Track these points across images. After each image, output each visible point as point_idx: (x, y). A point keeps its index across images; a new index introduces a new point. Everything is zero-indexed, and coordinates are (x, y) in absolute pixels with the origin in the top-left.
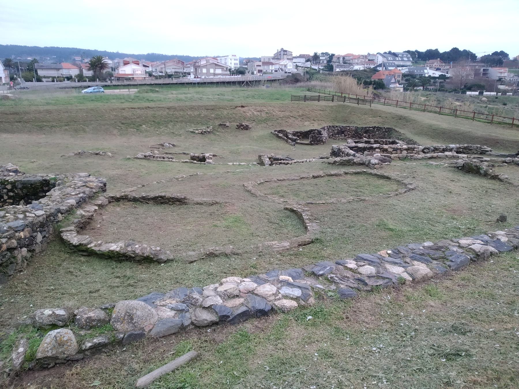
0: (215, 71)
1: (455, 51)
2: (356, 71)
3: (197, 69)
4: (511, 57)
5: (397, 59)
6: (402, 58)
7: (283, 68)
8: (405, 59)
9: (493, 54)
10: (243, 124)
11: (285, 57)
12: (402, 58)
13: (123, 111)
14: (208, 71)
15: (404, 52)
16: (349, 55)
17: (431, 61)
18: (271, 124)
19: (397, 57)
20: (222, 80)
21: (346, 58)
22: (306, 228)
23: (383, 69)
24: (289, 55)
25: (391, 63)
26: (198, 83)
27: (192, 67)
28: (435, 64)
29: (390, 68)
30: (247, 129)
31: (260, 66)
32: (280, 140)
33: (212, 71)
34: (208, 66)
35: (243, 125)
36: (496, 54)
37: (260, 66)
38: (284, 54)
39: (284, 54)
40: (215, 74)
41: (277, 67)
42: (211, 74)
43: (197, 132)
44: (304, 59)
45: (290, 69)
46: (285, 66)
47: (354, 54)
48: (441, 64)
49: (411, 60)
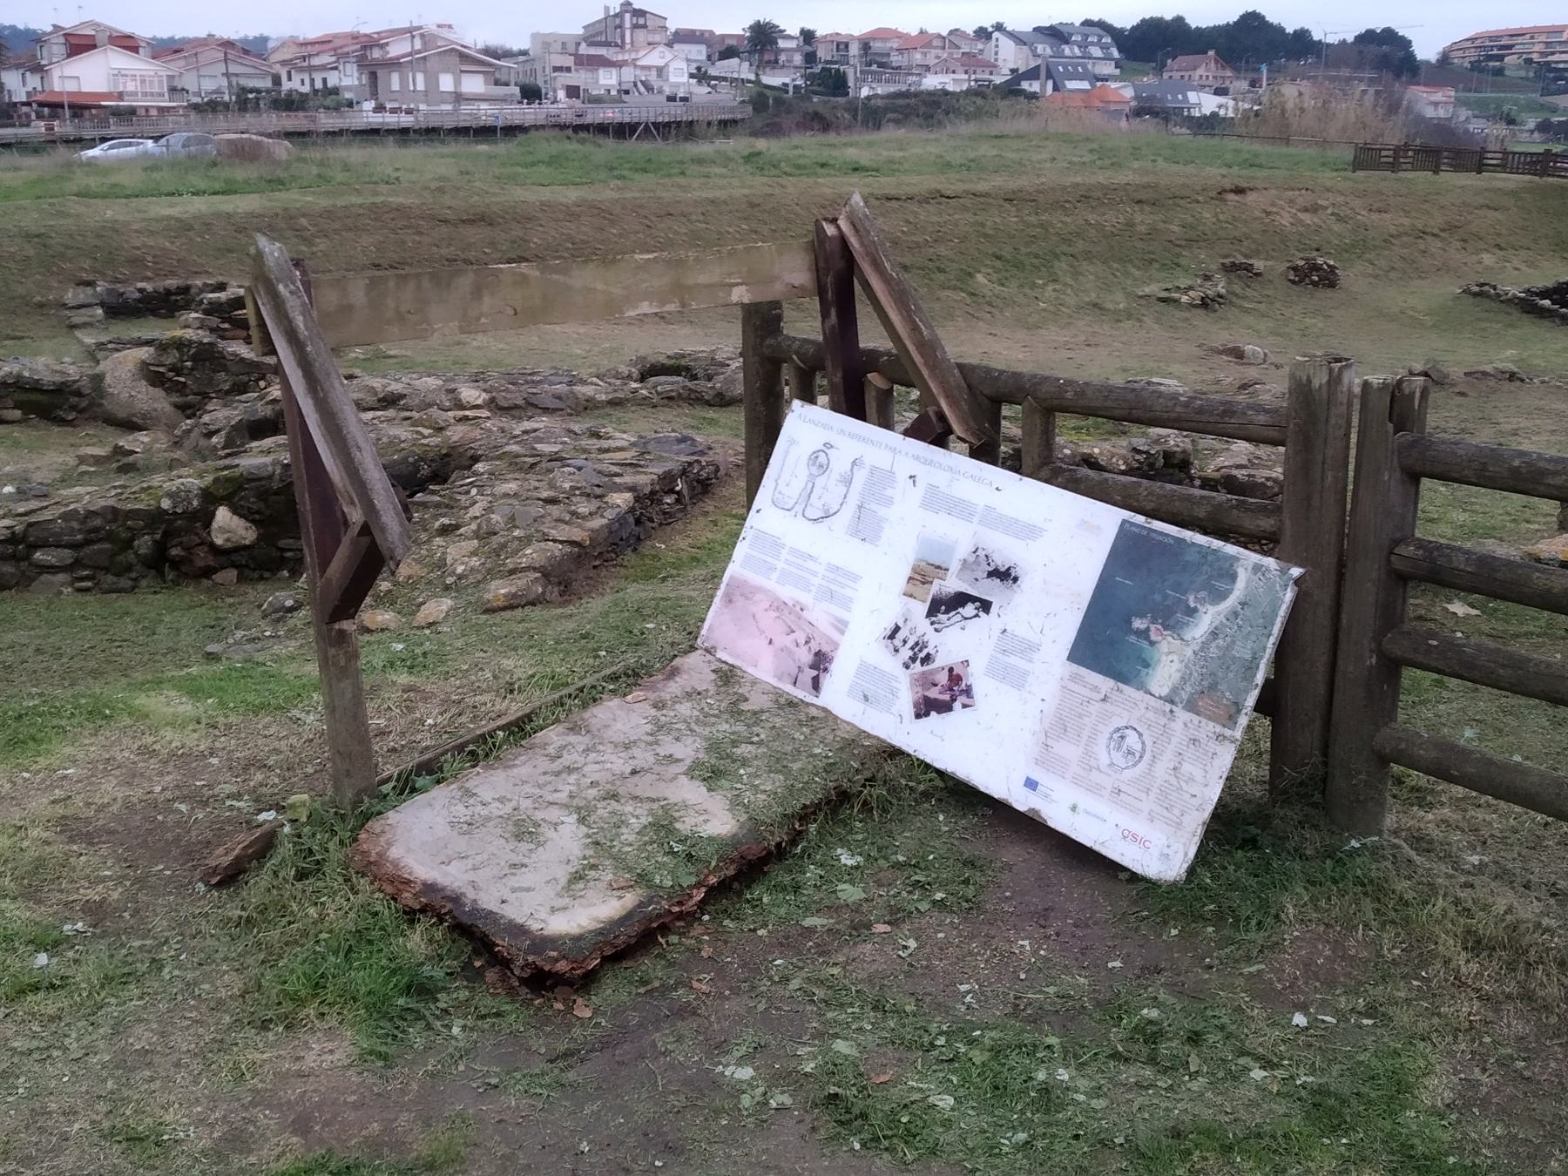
0: (457, 83)
1: (1252, 22)
2: (931, 93)
3: (380, 73)
4: (1426, 50)
5: (1067, 52)
6: (1084, 45)
7: (652, 77)
8: (1096, 52)
9: (1360, 39)
10: (1320, 261)
11: (641, 35)
12: (1084, 45)
13: (1007, 205)
14: (432, 81)
15: (1088, 23)
16: (883, 34)
17: (1183, 60)
18: (1383, 263)
19: (1067, 42)
20: (486, 120)
21: (877, 46)
22: (1098, 528)
23: (1043, 86)
24: (654, 31)
25: (1075, 66)
26: (404, 131)
27: (352, 69)
28: (1201, 71)
29: (1072, 85)
30: (1332, 285)
31: (568, 70)
32: (1546, 323)
33: (446, 83)
34: (432, 64)
35: (1316, 268)
36: (1368, 38)
37: (568, 70)
38: (635, 26)
39: (635, 26)
40: (458, 98)
41: (628, 74)
42: (443, 97)
43: (1184, 299)
44: (703, 48)
45: (678, 85)
46: (660, 71)
47: (903, 29)
48: (1221, 73)
49: (1116, 54)
